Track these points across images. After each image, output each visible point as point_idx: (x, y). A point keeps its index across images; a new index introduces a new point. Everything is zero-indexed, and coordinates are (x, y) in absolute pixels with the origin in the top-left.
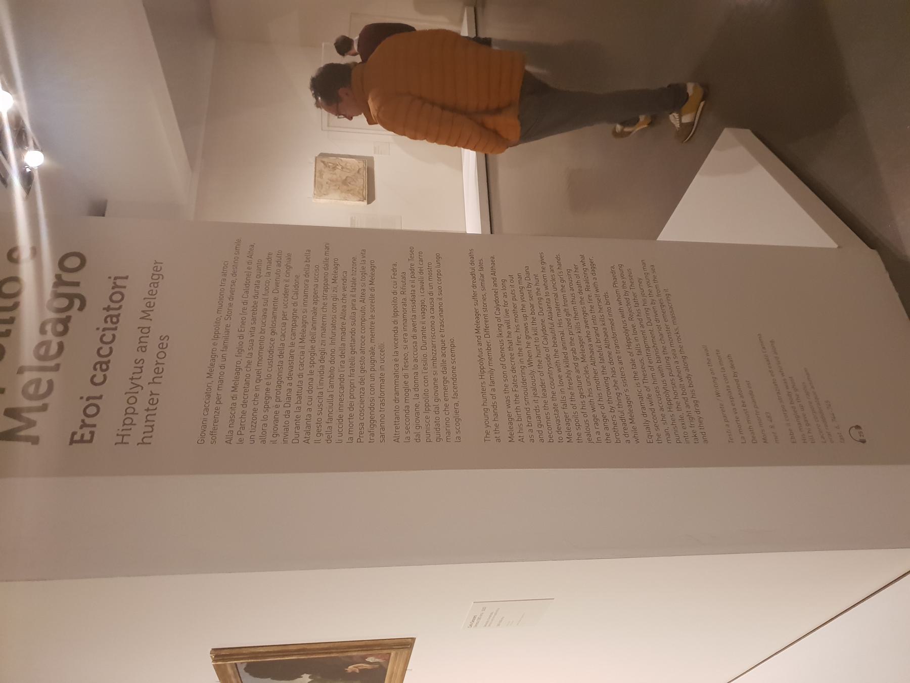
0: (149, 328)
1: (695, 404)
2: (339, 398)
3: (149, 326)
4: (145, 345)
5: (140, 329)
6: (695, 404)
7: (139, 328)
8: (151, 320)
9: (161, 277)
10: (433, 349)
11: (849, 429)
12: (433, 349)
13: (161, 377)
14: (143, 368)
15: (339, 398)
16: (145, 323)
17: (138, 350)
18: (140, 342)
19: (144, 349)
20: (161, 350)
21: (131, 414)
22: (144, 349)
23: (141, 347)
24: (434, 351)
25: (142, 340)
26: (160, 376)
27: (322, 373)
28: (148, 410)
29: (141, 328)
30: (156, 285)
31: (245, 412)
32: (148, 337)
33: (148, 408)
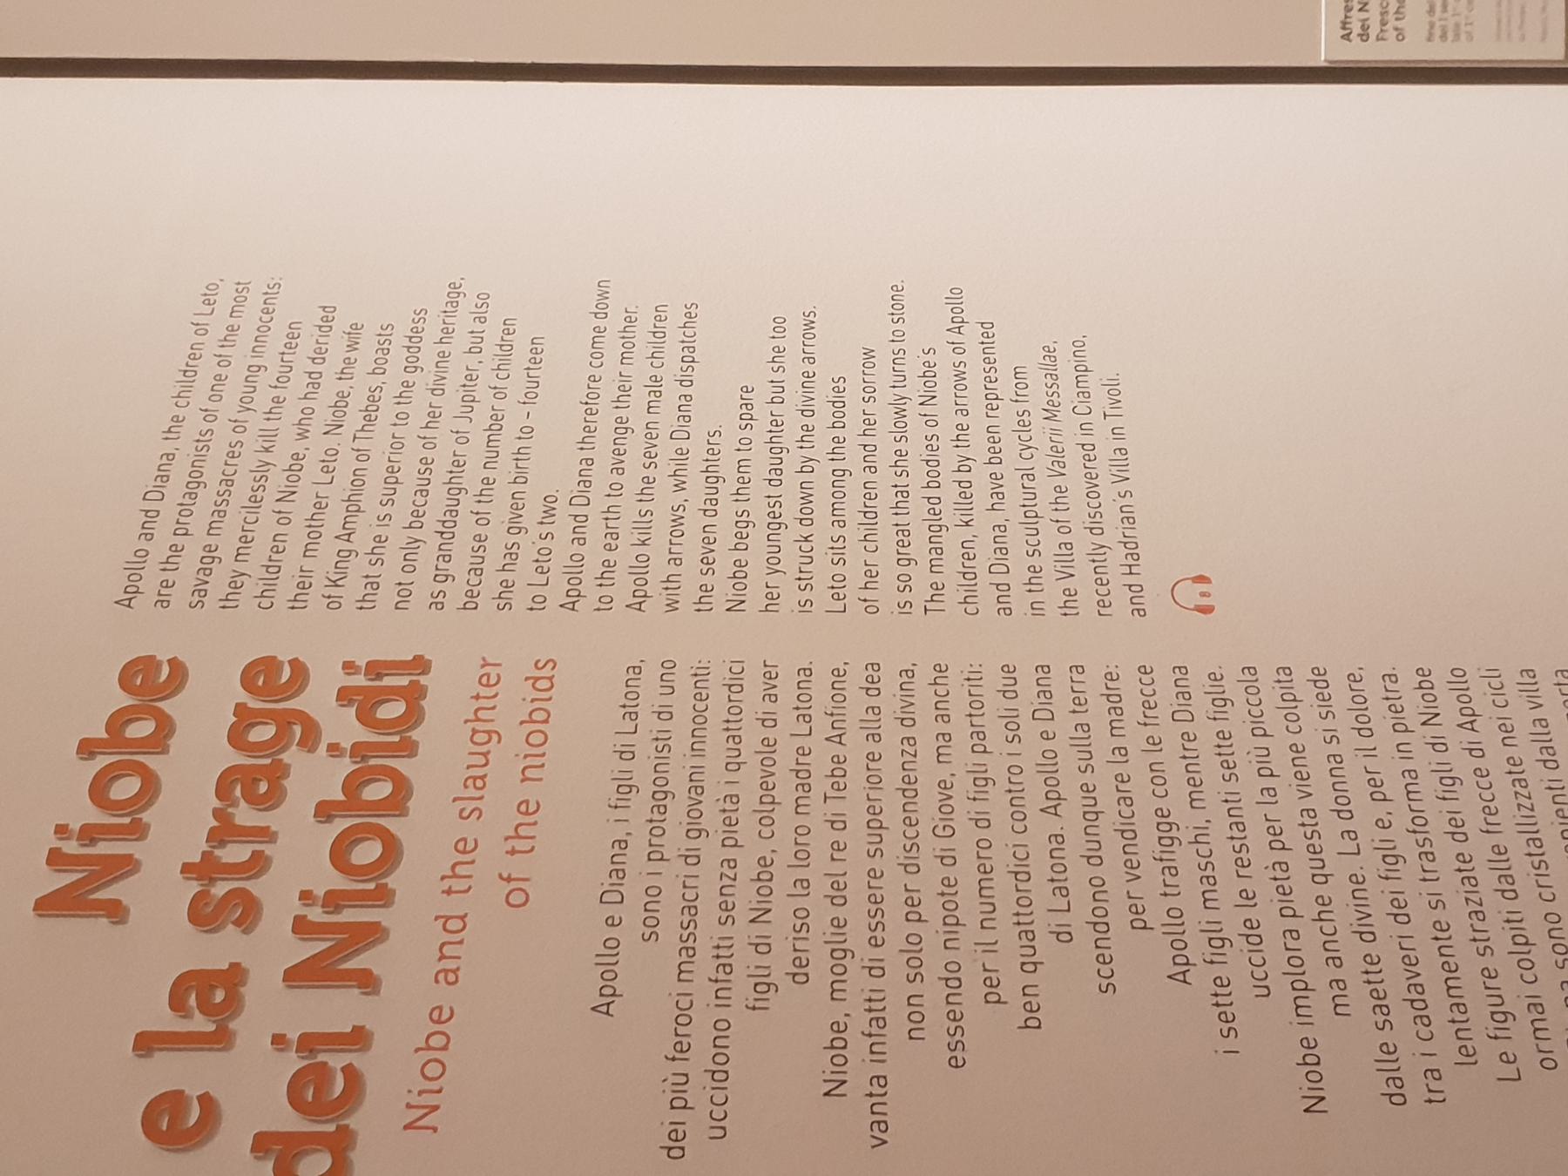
0: (463, 918)
1: (1281, 838)
2: (949, 1054)
3: (462, 914)
4: (455, 967)
5: (531, 681)
6: (1281, 838)
7: (527, 679)
8: (435, 1130)
9: (495, 737)
10: (1518, 789)
11: (937, 838)
12: (1518, 789)
13: (473, 862)
14: (521, 777)
15: (949, 1054)
16: (453, 905)
17: (437, 981)
18: (442, 957)
19: (451, 977)
20: (874, 817)
21: (767, 880)
22: (451, 977)
23: (446, 971)
24: (1527, 803)
25: (447, 950)
26: (469, 860)
27: (956, 983)
28: (477, 697)
29: (442, 917)
30: (479, 783)
31: (470, 846)
32: (461, 942)
33: (478, 694)
